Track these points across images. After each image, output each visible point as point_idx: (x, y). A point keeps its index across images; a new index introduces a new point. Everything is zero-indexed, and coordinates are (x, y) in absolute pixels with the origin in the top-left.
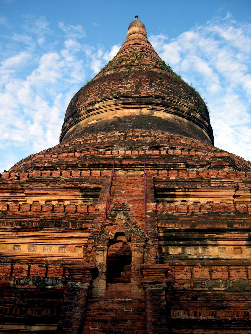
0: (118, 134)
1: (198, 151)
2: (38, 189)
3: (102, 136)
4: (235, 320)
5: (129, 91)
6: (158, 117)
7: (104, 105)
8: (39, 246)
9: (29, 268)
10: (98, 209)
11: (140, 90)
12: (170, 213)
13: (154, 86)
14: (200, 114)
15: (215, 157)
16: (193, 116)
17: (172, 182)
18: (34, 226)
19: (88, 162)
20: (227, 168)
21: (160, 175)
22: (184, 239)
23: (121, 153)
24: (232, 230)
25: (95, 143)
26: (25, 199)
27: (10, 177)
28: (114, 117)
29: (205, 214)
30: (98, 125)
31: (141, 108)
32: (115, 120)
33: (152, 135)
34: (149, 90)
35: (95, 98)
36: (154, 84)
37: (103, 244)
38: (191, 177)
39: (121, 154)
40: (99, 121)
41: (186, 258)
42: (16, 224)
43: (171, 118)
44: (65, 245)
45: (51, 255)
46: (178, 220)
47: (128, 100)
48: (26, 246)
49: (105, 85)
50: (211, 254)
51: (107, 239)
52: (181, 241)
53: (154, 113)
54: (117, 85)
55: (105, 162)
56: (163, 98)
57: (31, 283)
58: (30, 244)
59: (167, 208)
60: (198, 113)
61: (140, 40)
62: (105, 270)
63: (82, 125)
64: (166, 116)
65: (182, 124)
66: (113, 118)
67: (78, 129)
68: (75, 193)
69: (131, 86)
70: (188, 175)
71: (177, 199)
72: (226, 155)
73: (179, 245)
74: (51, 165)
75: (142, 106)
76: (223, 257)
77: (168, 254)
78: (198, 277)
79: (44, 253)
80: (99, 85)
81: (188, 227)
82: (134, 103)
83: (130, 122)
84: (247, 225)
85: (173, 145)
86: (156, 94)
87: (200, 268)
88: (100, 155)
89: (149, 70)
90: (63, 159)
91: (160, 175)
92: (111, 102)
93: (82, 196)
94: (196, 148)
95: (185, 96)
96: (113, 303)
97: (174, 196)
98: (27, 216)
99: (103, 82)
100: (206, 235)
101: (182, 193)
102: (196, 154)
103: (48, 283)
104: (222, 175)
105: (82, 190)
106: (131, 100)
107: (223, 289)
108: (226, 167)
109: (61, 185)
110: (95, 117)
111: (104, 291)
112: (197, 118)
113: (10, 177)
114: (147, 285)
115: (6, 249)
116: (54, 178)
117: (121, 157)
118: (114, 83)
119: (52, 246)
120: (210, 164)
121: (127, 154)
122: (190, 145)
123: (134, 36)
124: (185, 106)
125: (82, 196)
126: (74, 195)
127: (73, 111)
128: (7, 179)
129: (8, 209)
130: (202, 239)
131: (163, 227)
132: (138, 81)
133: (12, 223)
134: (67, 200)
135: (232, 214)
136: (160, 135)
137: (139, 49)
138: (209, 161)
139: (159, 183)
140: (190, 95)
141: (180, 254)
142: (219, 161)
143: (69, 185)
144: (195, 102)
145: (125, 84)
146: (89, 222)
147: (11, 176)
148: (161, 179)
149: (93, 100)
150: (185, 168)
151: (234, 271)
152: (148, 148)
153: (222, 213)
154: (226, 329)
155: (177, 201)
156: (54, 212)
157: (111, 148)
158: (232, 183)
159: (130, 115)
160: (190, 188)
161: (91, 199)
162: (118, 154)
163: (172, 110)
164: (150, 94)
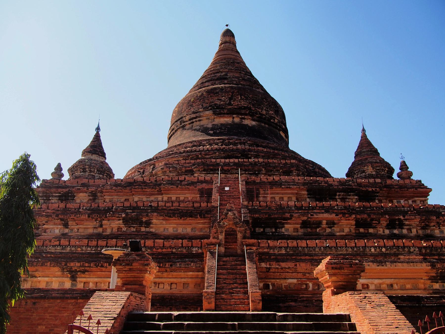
28: (213, 125)
56: (250, 109)
73: (261, 227)
98: (171, 210)
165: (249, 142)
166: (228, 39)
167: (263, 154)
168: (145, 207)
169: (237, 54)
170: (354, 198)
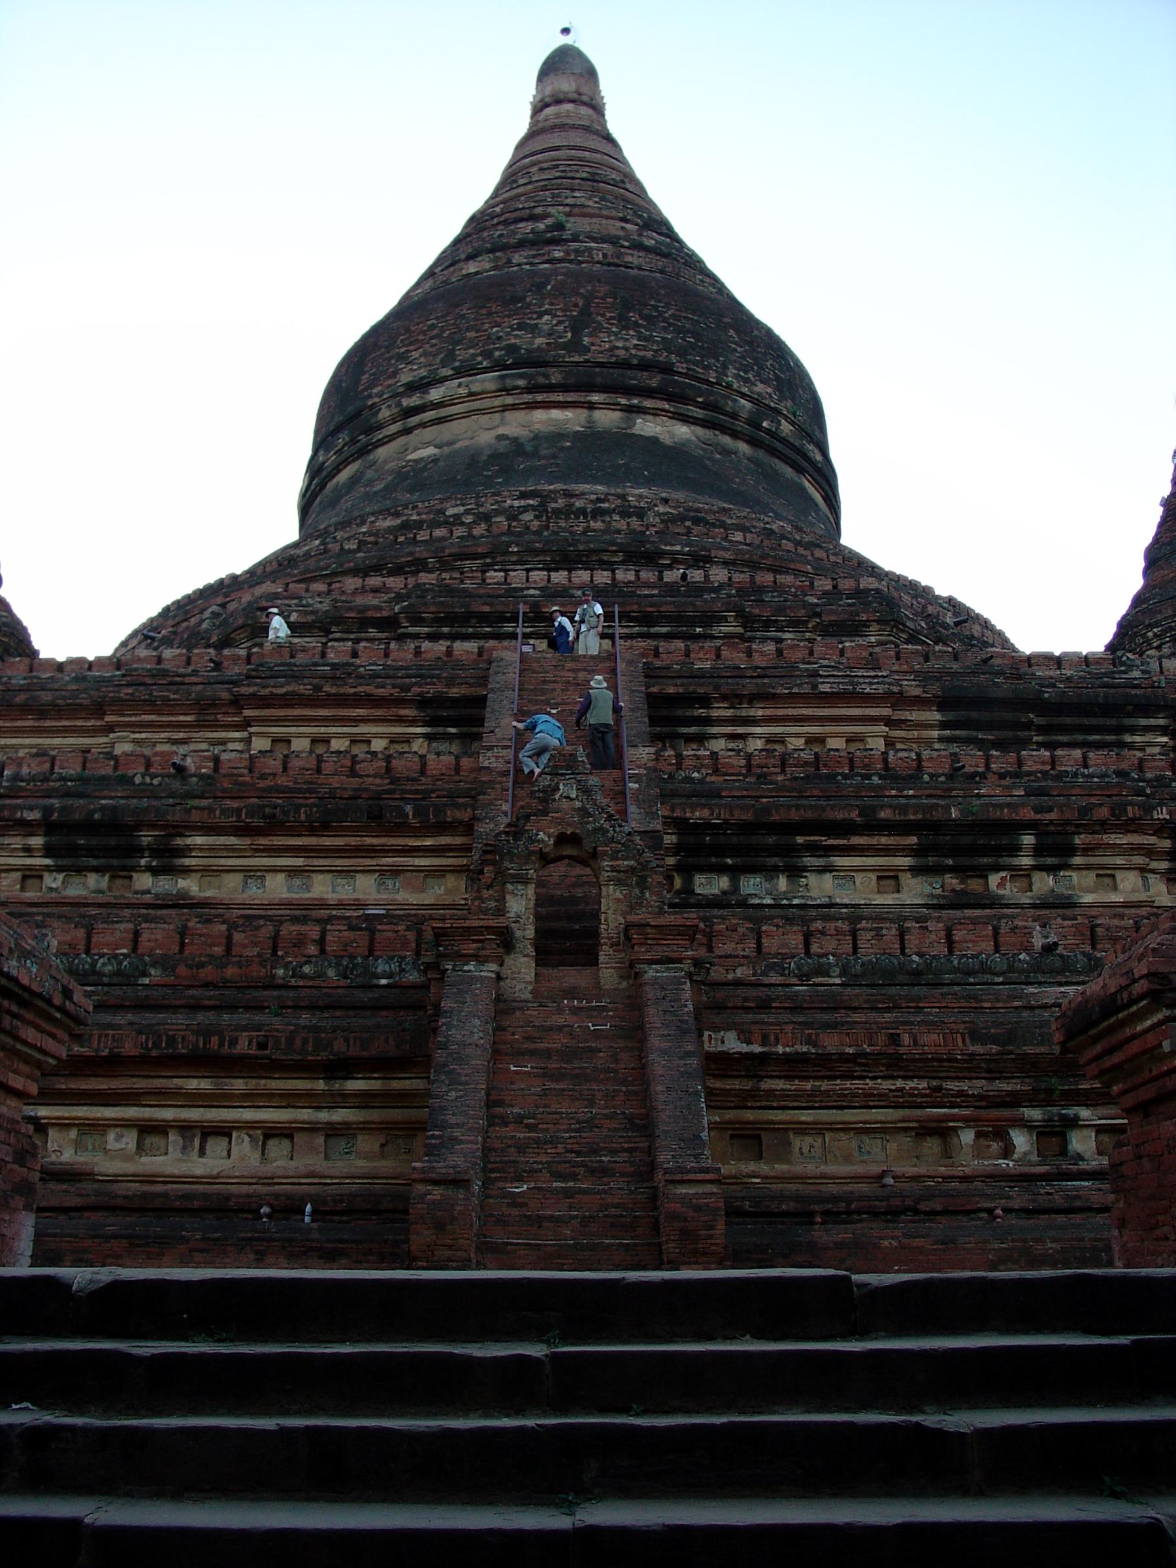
0: (516, 503)
1: (781, 573)
2: (288, 701)
3: (462, 509)
4: (865, 1055)
5: (547, 344)
6: (648, 438)
7: (463, 391)
8: (321, 877)
9: (323, 933)
10: (486, 764)
11: (586, 341)
12: (696, 775)
13: (636, 323)
14: (792, 423)
15: (835, 593)
16: (768, 431)
17: (701, 675)
18: (303, 817)
19: (432, 609)
20: (875, 627)
21: (664, 656)
22: (736, 851)
23: (537, 578)
24: (873, 827)
25: (443, 539)
26: (245, 734)
27: (189, 662)
28: (500, 438)
29: (796, 778)
30: (441, 464)
31: (591, 406)
32: (503, 447)
33: (630, 506)
34: (618, 340)
35: (430, 365)
36: (633, 316)
37: (526, 863)
38: (758, 660)
39: (535, 582)
40: (446, 450)
41: (743, 904)
42: (251, 814)
43: (694, 438)
44: (396, 872)
45: (355, 900)
46: (507, 553)
47: (546, 376)
48: (281, 877)
49: (463, 317)
50: (812, 894)
51: (533, 852)
52: (728, 857)
53: (635, 424)
54: (506, 320)
55: (487, 609)
56: (666, 369)
57: (331, 973)
58: (292, 872)
59: (688, 763)
60: (786, 418)
61: (581, 133)
62: (530, 932)
63: (385, 462)
64: (677, 432)
65: (731, 461)
66: (493, 441)
67: (370, 474)
68: (403, 712)
69: (555, 322)
70: (749, 653)
71: (715, 730)
72: (871, 587)
73: (721, 869)
74: (310, 618)
75: (595, 398)
76: (846, 901)
77: (692, 892)
78: (774, 950)
79: (335, 896)
80: (443, 317)
81: (748, 816)
82: (564, 388)
83: (554, 457)
84: (915, 814)
85: (703, 548)
86: (641, 354)
87: (777, 926)
88: (468, 585)
89: (616, 261)
90: (349, 598)
91: (664, 656)
92: (486, 381)
93: (423, 721)
94: (774, 557)
95: (743, 357)
96: (560, 1011)
97: (708, 721)
98: (277, 789)
99: (457, 306)
100: (800, 840)
101: (730, 713)
102: (775, 582)
103: (379, 970)
104: (854, 655)
105: (423, 703)
106: (556, 377)
107: (838, 981)
108: (869, 627)
109: (360, 689)
110: (429, 433)
111: (530, 988)
112: (783, 438)
113: (189, 662)
114: (645, 967)
115: (219, 888)
116: (334, 666)
117: (537, 592)
118: (493, 310)
119: (358, 875)
120: (818, 615)
121: (556, 581)
122: (759, 546)
123: (558, 116)
124: (743, 395)
125: (423, 721)
126: (400, 720)
127: (350, 409)
128: (182, 671)
129: (216, 769)
130: (793, 851)
131: (677, 818)
132: (581, 304)
133: (238, 811)
134: (377, 736)
135: (875, 780)
136: (656, 505)
137: (577, 171)
138: (817, 605)
139: (661, 680)
140: (760, 356)
141: (724, 893)
142: (849, 605)
143: (383, 687)
144: (778, 378)
145: (535, 316)
146: (464, 806)
147: (194, 659)
148: (668, 668)
149: (423, 372)
150: (741, 630)
151: (870, 935)
152: (620, 557)
153: (845, 777)
154: (841, 1077)
155: (715, 737)
156: (361, 776)
157: (498, 559)
158: (883, 683)
159: (553, 428)
160: (754, 699)
161: (453, 730)
162: (527, 580)
163: (699, 413)
164: (621, 353)
165: (661, 509)
166: (565, 84)
167: (728, 555)
168: (153, 777)
169: (608, 148)
170: (1152, 744)
